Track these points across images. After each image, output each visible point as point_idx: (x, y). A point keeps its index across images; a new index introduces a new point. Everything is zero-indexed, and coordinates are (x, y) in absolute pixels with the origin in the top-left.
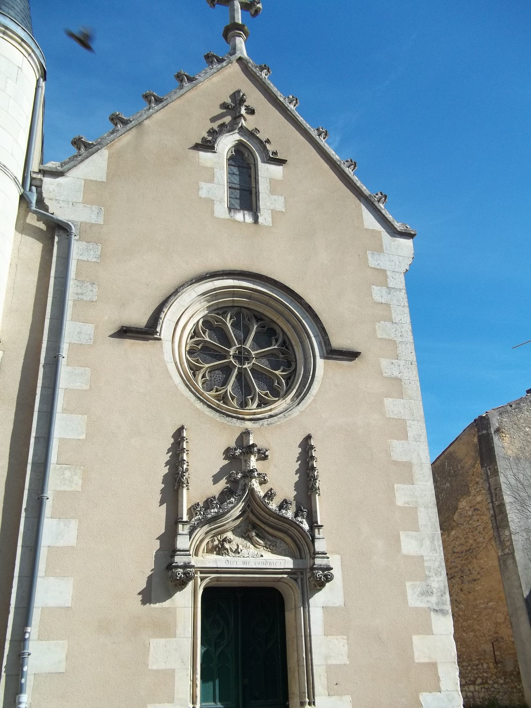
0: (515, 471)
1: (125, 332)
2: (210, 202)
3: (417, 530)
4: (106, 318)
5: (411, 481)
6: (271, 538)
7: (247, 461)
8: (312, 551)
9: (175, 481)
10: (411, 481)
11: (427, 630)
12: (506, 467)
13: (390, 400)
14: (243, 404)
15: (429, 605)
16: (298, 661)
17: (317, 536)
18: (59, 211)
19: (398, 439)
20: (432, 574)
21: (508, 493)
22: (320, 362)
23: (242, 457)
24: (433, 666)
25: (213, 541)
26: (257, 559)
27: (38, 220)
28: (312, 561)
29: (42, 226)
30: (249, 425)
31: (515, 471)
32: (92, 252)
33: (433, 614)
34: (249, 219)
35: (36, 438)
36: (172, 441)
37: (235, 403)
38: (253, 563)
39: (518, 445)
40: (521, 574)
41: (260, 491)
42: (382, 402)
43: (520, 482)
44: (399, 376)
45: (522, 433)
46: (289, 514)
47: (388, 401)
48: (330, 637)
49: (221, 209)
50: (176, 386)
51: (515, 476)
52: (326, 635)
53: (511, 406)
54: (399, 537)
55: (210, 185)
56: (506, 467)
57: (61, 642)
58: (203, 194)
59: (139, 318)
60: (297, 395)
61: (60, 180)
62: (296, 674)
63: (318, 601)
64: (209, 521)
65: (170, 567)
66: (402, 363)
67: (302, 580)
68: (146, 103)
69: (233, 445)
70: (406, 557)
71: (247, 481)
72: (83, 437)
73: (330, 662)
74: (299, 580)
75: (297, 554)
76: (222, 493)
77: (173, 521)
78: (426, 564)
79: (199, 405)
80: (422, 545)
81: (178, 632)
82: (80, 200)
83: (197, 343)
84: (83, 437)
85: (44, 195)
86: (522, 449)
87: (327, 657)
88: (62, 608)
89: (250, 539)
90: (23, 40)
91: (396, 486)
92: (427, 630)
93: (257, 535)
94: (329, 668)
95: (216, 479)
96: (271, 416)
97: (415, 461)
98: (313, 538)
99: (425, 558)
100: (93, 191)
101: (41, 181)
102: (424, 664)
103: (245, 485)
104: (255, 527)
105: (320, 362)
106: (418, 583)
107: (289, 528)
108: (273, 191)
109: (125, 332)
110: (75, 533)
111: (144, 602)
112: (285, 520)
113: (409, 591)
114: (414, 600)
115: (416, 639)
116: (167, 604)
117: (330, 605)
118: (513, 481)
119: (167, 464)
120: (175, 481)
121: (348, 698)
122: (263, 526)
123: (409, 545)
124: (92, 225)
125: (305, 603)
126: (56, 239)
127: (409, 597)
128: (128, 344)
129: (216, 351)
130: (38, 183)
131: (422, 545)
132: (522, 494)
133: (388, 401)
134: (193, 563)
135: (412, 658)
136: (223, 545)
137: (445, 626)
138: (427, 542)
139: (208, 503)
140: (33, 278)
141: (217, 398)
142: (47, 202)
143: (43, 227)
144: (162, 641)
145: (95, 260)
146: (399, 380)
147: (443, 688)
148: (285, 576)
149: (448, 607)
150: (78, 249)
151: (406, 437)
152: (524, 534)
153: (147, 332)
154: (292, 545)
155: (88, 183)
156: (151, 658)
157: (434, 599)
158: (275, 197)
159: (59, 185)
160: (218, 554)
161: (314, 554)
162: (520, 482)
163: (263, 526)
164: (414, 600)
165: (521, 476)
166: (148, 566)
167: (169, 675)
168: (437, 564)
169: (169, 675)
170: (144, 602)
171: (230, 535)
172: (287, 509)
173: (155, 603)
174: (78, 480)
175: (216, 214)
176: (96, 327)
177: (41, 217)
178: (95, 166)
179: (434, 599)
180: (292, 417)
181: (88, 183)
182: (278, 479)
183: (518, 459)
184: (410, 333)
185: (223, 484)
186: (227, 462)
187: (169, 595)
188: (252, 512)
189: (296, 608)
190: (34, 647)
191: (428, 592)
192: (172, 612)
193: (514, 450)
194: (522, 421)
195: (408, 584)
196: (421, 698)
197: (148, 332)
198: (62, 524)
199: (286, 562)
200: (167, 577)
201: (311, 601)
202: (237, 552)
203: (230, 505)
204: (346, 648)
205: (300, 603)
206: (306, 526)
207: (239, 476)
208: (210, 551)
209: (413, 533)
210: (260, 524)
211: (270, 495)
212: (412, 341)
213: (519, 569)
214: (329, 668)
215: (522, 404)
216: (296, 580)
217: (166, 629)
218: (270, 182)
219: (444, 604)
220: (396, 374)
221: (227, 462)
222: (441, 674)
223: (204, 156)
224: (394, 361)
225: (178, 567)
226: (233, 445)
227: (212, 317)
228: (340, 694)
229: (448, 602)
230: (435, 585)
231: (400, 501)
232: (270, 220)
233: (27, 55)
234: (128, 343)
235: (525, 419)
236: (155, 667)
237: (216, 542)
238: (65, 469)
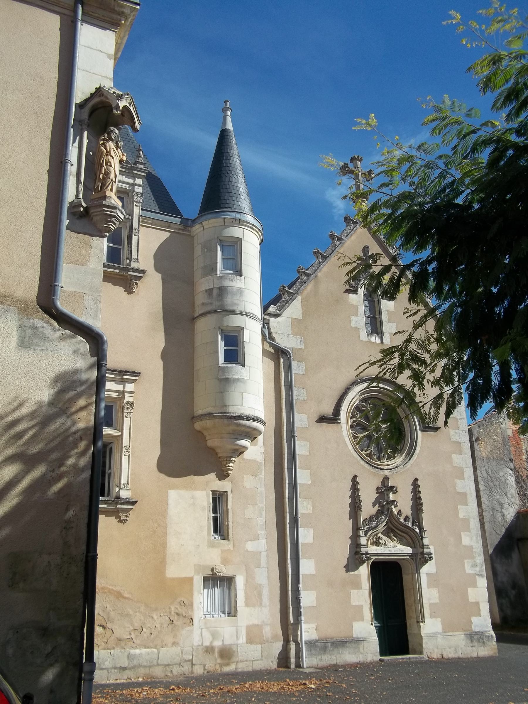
0: (487, 468)
1: (322, 419)
2: (357, 329)
3: (469, 531)
4: (312, 410)
5: (466, 503)
6: (400, 537)
7: (388, 495)
8: (421, 544)
9: (355, 506)
10: (466, 503)
11: (475, 585)
12: (481, 465)
13: (455, 455)
14: (379, 459)
15: (475, 572)
16: (415, 601)
17: (424, 536)
18: (283, 342)
19: (459, 479)
20: (477, 555)
21: (482, 483)
22: (419, 433)
23: (385, 492)
24: (477, 603)
25: (373, 539)
26: (394, 548)
27: (270, 347)
28: (421, 550)
29: (271, 350)
30: (387, 473)
31: (487, 468)
32: (301, 368)
33: (477, 577)
34: (378, 341)
35: (288, 484)
36: (351, 483)
37: (375, 458)
38: (393, 551)
39: (489, 449)
40: (488, 538)
41: (395, 511)
42: (451, 457)
43: (489, 475)
44: (460, 440)
45: (492, 441)
46: (409, 524)
47: (454, 456)
48: (430, 589)
49: (363, 335)
50: (350, 451)
51: (486, 471)
52: (428, 588)
53: (486, 421)
54: (461, 535)
55: (356, 318)
56: (481, 465)
57: (313, 591)
58: (353, 324)
59: (328, 409)
60: (408, 454)
61: (279, 319)
62: (413, 607)
63: (426, 569)
64: (373, 529)
65: (357, 553)
66: (461, 432)
67: (416, 559)
68: (315, 258)
69: (380, 485)
70: (465, 546)
71: (389, 506)
72: (310, 482)
73: (432, 601)
74: (414, 559)
75: (413, 545)
76: (377, 513)
77: (356, 529)
78: (474, 550)
79: (362, 462)
80: (472, 540)
81: (362, 587)
82: (290, 333)
83: (354, 422)
84: (310, 482)
85: (272, 330)
86: (491, 452)
87: (429, 599)
88: (311, 574)
89: (389, 537)
90: (253, 225)
91: (459, 507)
92: (475, 585)
93: (394, 535)
94: (431, 605)
95: (374, 505)
96: (396, 467)
97: (468, 492)
98: (422, 538)
99: (474, 547)
100: (297, 325)
101: (269, 320)
102: (473, 602)
103: (388, 509)
104: (392, 531)
105: (419, 433)
106: (470, 560)
107: (408, 531)
108: (390, 321)
109: (322, 419)
110: (312, 535)
111: (347, 571)
112: (408, 527)
113: (466, 565)
114: (469, 570)
115: (470, 590)
116: (356, 572)
117: (430, 572)
118: (485, 475)
119: (350, 497)
120: (355, 506)
121: (439, 619)
122: (396, 530)
123: (466, 540)
124: (299, 349)
125: (418, 571)
126: (282, 360)
127: (466, 568)
128: (325, 426)
129: (365, 427)
130: (267, 322)
131: (472, 540)
132: (490, 484)
133: (454, 456)
134: (369, 552)
135: (468, 599)
136: (378, 541)
137: (483, 583)
138: (474, 538)
139: (371, 519)
140: (272, 385)
141: (367, 455)
142: (274, 335)
143: (273, 351)
144: (356, 591)
145: (303, 373)
146: (459, 443)
147: (482, 615)
148: (408, 557)
149: (484, 573)
150: (297, 368)
151: (463, 478)
152: (491, 512)
153: (332, 419)
154: (410, 541)
155: (294, 321)
156: (352, 600)
157: (478, 569)
158: (391, 324)
159: (278, 322)
160: (376, 546)
161: (423, 546)
162: (489, 475)
163: (396, 530)
164: (469, 570)
165: (490, 471)
166: (346, 552)
167: (361, 607)
168: (479, 550)
169: (361, 607)
170: (347, 571)
171: (380, 535)
172: (408, 521)
173: (352, 572)
174: (310, 507)
175: (361, 338)
176: (308, 417)
177: (271, 345)
178: (294, 309)
179: (478, 569)
180: (407, 468)
181: (294, 321)
182: (403, 503)
183: (489, 459)
184: (465, 413)
185: (377, 507)
186: (378, 495)
187: (357, 568)
188: (391, 522)
189: (412, 574)
190: (303, 594)
191: (475, 565)
192: (359, 576)
193: (487, 453)
194: (492, 431)
195: (466, 561)
196: (472, 620)
197: (332, 419)
198: (306, 531)
199: (408, 550)
200: (356, 557)
201: (421, 570)
202: (385, 544)
203: (382, 520)
204: (438, 595)
205: (415, 572)
206: (418, 531)
207: (385, 503)
208: (372, 544)
209: (468, 533)
210: (396, 530)
211: (400, 513)
212: (465, 418)
213: (487, 535)
214: (431, 605)
215: (493, 419)
216: (412, 559)
217: (357, 585)
218: (388, 313)
219: (482, 571)
220: (458, 439)
221: (378, 495)
222: (481, 608)
223: (351, 296)
224: (457, 431)
225: (363, 554)
226: (380, 485)
227: (360, 404)
228: (435, 617)
229: (485, 571)
230: (478, 561)
231: (461, 516)
232: (389, 340)
233: (250, 229)
234: (325, 425)
235: (494, 430)
236: (354, 604)
237: (375, 540)
238: (304, 501)
